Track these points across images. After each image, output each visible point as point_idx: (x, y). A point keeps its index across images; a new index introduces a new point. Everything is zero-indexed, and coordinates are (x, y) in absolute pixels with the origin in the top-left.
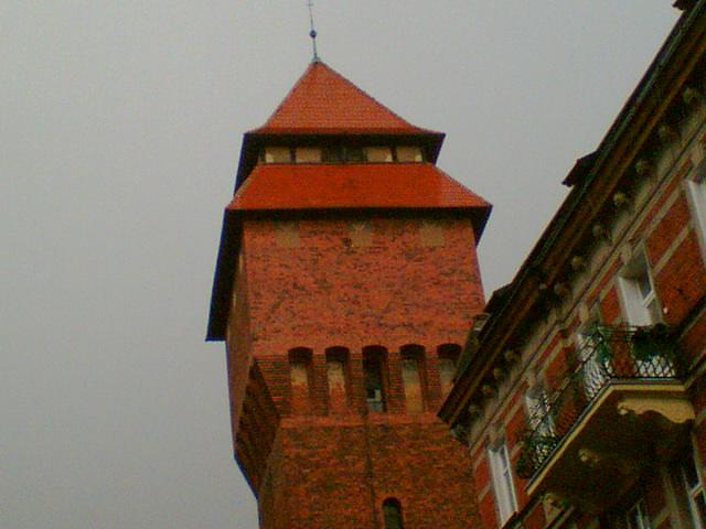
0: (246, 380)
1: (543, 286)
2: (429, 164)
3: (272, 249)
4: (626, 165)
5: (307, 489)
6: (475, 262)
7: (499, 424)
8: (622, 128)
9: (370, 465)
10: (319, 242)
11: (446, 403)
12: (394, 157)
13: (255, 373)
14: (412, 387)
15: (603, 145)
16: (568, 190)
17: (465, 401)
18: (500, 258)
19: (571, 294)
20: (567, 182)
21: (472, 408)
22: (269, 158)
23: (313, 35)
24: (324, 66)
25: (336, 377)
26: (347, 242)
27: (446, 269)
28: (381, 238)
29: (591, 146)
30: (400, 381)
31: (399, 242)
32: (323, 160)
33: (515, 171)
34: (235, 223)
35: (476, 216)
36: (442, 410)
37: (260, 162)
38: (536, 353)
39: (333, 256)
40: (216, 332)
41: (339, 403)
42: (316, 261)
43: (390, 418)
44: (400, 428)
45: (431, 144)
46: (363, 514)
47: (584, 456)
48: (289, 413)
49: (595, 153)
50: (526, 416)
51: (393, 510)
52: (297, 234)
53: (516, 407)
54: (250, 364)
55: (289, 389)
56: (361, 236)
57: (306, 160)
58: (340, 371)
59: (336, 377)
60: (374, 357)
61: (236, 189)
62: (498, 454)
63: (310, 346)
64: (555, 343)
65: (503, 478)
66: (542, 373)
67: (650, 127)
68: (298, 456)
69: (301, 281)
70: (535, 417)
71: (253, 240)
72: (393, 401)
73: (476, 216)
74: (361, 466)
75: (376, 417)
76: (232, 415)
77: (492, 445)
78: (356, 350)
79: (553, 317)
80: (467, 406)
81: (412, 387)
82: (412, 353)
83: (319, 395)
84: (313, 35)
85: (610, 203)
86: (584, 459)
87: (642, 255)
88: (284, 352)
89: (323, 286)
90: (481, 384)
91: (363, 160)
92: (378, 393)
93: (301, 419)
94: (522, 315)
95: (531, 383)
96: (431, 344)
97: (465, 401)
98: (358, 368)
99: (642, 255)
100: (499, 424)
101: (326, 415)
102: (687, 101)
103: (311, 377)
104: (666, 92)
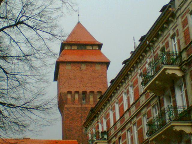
1: (95, 114)
2: (99, 50)
3: (66, 69)
5: (69, 120)
6: (106, 73)
9: (82, 115)
10: (75, 68)
11: (98, 102)
12: (92, 48)
14: (92, 99)
15: (116, 77)
16: (161, 13)
17: (122, 79)
18: (112, 73)
19: (169, 27)
20: (140, 41)
22: (66, 48)
23: (79, 15)
24: (80, 23)
25: (76, 96)
26: (80, 68)
27: (100, 75)
28: (87, 67)
31: (91, 69)
32: (77, 48)
33: (117, 52)
34: (58, 64)
37: (64, 49)
38: (167, 33)
39: (77, 71)
40: (56, 79)
42: (74, 73)
45: (100, 46)
46: (80, 125)
48: (67, 104)
49: (114, 79)
50: (93, 133)
52: (70, 66)
53: (121, 96)
55: (67, 100)
56: (84, 67)
57: (74, 49)
60: (84, 93)
61: (60, 54)
63: (71, 91)
64: (96, 123)
66: (142, 71)
69: (71, 77)
70: (160, 56)
71: (61, 67)
72: (88, 102)
74: (80, 115)
75: (84, 106)
77: (130, 86)
78: (81, 92)
79: (97, 119)
80: (106, 101)
81: (92, 99)
82: (92, 92)
83: (73, 101)
84: (79, 15)
86: (157, 83)
87: (164, 46)
89: (75, 78)
90: (137, 60)
91: (86, 48)
92: (85, 100)
93: (69, 105)
96: (96, 91)
97: (122, 79)
98: (81, 96)
99: (164, 46)
100: (117, 99)
101: (74, 105)
103: (71, 96)
104: (106, 98)
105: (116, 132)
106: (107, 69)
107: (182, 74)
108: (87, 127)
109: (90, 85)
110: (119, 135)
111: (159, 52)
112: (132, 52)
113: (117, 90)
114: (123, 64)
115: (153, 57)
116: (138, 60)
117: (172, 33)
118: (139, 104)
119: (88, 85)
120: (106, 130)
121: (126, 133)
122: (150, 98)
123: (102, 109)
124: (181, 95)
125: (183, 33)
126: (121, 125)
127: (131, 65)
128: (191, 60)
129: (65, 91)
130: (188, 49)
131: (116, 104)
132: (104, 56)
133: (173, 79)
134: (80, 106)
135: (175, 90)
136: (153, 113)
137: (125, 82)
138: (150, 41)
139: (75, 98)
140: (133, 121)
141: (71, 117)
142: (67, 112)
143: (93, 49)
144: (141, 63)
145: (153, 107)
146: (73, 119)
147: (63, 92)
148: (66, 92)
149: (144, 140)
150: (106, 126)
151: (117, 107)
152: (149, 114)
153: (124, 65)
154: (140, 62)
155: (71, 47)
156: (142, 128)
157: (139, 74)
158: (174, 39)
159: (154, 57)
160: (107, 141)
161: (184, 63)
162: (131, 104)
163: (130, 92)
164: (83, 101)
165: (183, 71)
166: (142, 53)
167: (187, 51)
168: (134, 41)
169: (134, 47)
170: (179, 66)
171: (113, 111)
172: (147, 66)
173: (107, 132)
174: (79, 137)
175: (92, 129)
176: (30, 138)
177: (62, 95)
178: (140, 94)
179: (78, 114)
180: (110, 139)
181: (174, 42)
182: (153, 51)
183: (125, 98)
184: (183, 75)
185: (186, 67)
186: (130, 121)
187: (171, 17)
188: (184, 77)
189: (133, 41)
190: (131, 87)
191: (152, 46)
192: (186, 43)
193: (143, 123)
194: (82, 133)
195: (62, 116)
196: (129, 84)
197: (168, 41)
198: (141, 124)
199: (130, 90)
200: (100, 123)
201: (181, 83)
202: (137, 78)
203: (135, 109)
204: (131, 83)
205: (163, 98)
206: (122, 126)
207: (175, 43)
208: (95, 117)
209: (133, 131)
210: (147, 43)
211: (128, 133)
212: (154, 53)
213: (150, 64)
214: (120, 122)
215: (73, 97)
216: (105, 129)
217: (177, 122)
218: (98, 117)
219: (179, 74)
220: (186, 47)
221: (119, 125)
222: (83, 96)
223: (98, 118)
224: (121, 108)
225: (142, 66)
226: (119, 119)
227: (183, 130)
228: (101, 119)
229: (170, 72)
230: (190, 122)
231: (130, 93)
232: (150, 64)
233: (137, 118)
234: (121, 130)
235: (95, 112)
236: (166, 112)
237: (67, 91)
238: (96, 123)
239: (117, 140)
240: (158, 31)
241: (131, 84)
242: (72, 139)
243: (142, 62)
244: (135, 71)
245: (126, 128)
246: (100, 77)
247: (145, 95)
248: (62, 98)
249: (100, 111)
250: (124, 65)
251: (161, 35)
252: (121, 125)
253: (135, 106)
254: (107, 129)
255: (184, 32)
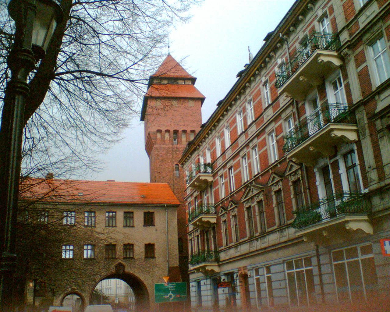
0: (147, 135)
1: (195, 146)
4: (235, 96)
6: (200, 111)
7: (227, 122)
8: (228, 96)
12: (185, 83)
13: (149, 134)
18: (207, 111)
19: (271, 61)
20: (264, 40)
21: (225, 113)
24: (171, 56)
29: (222, 98)
30: (181, 138)
31: (183, 105)
33: (214, 83)
34: (146, 99)
35: (202, 100)
36: (180, 161)
40: (142, 119)
41: (167, 142)
43: (179, 146)
44: (181, 148)
45: (193, 80)
47: (196, 183)
51: (177, 166)
54: (148, 132)
55: (156, 139)
58: (168, 135)
59: (167, 136)
60: (176, 132)
62: (218, 140)
64: (197, 157)
65: (228, 136)
67: (239, 90)
68: (157, 154)
71: (151, 103)
72: (179, 142)
73: (202, 100)
74: (171, 156)
75: (175, 146)
76: (145, 133)
77: (247, 101)
78: (172, 131)
81: (184, 139)
82: (184, 131)
84: (169, 47)
85: (276, 46)
88: (155, 130)
91: (177, 83)
92: (176, 140)
94: (192, 150)
95: (217, 135)
98: (172, 135)
100: (227, 122)
102: (242, 92)
103: (161, 135)
104: (212, 123)
105: (247, 141)
106: (201, 106)
107: (339, 63)
108: (186, 160)
109: (183, 124)
110: (229, 165)
111: (297, 45)
112: (246, 65)
113: (227, 110)
114: (237, 77)
115: (287, 55)
116: (263, 64)
117: (320, 13)
118: (263, 121)
119: (180, 124)
120: (210, 162)
121: (267, 138)
122: (249, 139)
123: (205, 138)
124: (335, 94)
125: (342, 7)
126: (232, 152)
127: (251, 73)
128: (389, 9)
129: (154, 129)
130: (350, 27)
131: (192, 165)
132: (198, 91)
133: (329, 68)
134: (171, 146)
135: (325, 89)
136: (285, 128)
137: (211, 133)
138: (283, 33)
139: (166, 138)
140: (251, 145)
141: (161, 158)
142: (156, 153)
143: (186, 84)
144: (260, 76)
145: (285, 120)
146: (163, 161)
147: (152, 131)
148: (156, 131)
149: (270, 164)
150: (210, 158)
151: (227, 133)
152: (279, 130)
153: (238, 78)
154: (265, 66)
155: (161, 81)
156: (266, 150)
157: (263, 83)
158: (266, 86)
159: (289, 54)
160: (211, 175)
161: (347, 45)
162: (249, 122)
163: (247, 109)
164: (174, 141)
165: (342, 58)
166: (270, 53)
167: (348, 30)
168: (249, 51)
169: (250, 59)
170: (337, 51)
171: (204, 157)
172: (276, 69)
173: (212, 165)
174: (170, 179)
175: (233, 115)
176: (114, 181)
177: (151, 134)
178: (264, 108)
179: (169, 155)
180: (215, 172)
181: (266, 89)
182: (288, 46)
183: (239, 119)
184: (342, 64)
185: (348, 50)
186: (247, 145)
187: (301, 15)
188: (343, 68)
189: (248, 51)
190: (248, 103)
191: (286, 40)
192: (347, 20)
193: (267, 144)
194: (173, 175)
195: (149, 158)
196: (237, 110)
197: (314, 25)
198: (266, 145)
199: (247, 107)
200: (202, 157)
201: (339, 74)
202: (260, 88)
203: (231, 152)
204: (248, 98)
205: (304, 105)
206: (258, 130)
207: (268, 90)
208: (195, 150)
209: (251, 156)
210: (279, 35)
211: (242, 160)
212: (289, 49)
213: (280, 66)
214: (231, 149)
215: (163, 137)
216: (209, 160)
217: (337, 124)
218: (198, 149)
219: (337, 62)
220: (346, 25)
221: (229, 154)
222: (174, 135)
223: (199, 151)
224: (233, 133)
225: (267, 72)
226: (231, 146)
227: (345, 135)
228: (203, 152)
229: (326, 59)
230: (355, 124)
231: (247, 111)
232: (280, 66)
233: (224, 170)
234: (383, 20)
235: (196, 143)
236: (308, 121)
237: (157, 129)
238: (197, 157)
239: (226, 171)
240: (299, 16)
241: (250, 99)
242: (162, 182)
243: (268, 66)
244: (256, 80)
245: (240, 155)
246: (193, 115)
247: (273, 107)
248: (151, 138)
249: (202, 142)
250: (238, 78)
251: (302, 20)
252: (232, 152)
253: (255, 125)
254: (211, 161)
255: (343, 5)
